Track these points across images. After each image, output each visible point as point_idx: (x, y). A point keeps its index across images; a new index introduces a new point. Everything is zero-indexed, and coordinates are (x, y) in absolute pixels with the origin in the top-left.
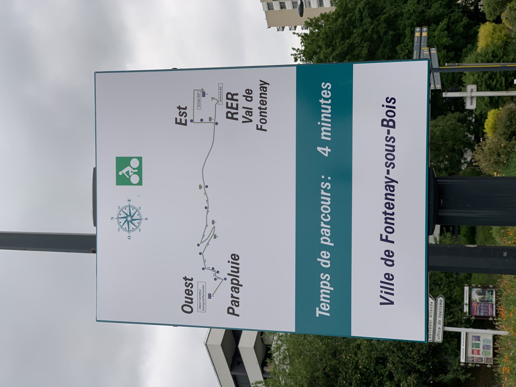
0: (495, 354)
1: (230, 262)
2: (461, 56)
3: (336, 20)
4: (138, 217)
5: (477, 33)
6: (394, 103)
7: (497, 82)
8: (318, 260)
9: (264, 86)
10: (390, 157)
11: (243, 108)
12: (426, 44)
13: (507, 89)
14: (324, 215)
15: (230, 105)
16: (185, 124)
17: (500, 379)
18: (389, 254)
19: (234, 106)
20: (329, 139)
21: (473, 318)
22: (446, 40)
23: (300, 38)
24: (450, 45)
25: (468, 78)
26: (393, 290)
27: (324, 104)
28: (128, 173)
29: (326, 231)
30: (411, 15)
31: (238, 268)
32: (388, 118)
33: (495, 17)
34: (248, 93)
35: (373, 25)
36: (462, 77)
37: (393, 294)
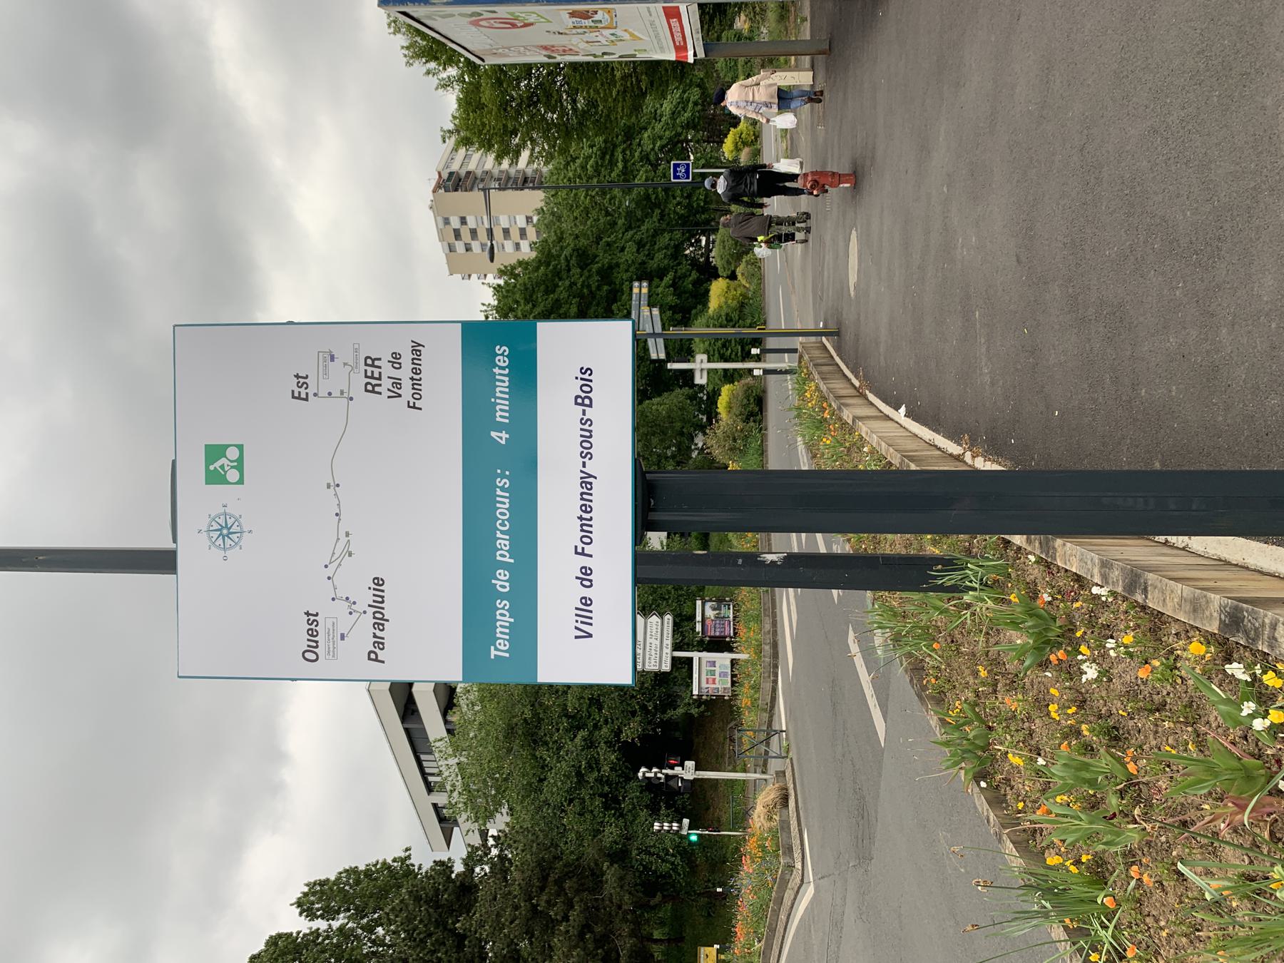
0: (733, 683)
2: (689, 319)
3: (537, 269)
4: (212, 534)
5: (708, 291)
6: (590, 375)
7: (732, 351)
8: (493, 581)
9: (417, 349)
10: (585, 445)
11: (389, 377)
12: (646, 302)
13: (743, 360)
14: (500, 521)
16: (306, 399)
17: (739, 714)
18: (586, 571)
19: (376, 375)
20: (507, 421)
21: (708, 639)
22: (671, 299)
23: (492, 289)
24: (676, 305)
25: (698, 345)
26: (591, 618)
27: (500, 374)
28: (222, 467)
29: (503, 542)
30: (629, 266)
31: (382, 597)
32: (583, 395)
33: (729, 273)
34: (396, 358)
35: (583, 278)
36: (690, 344)
37: (591, 624)
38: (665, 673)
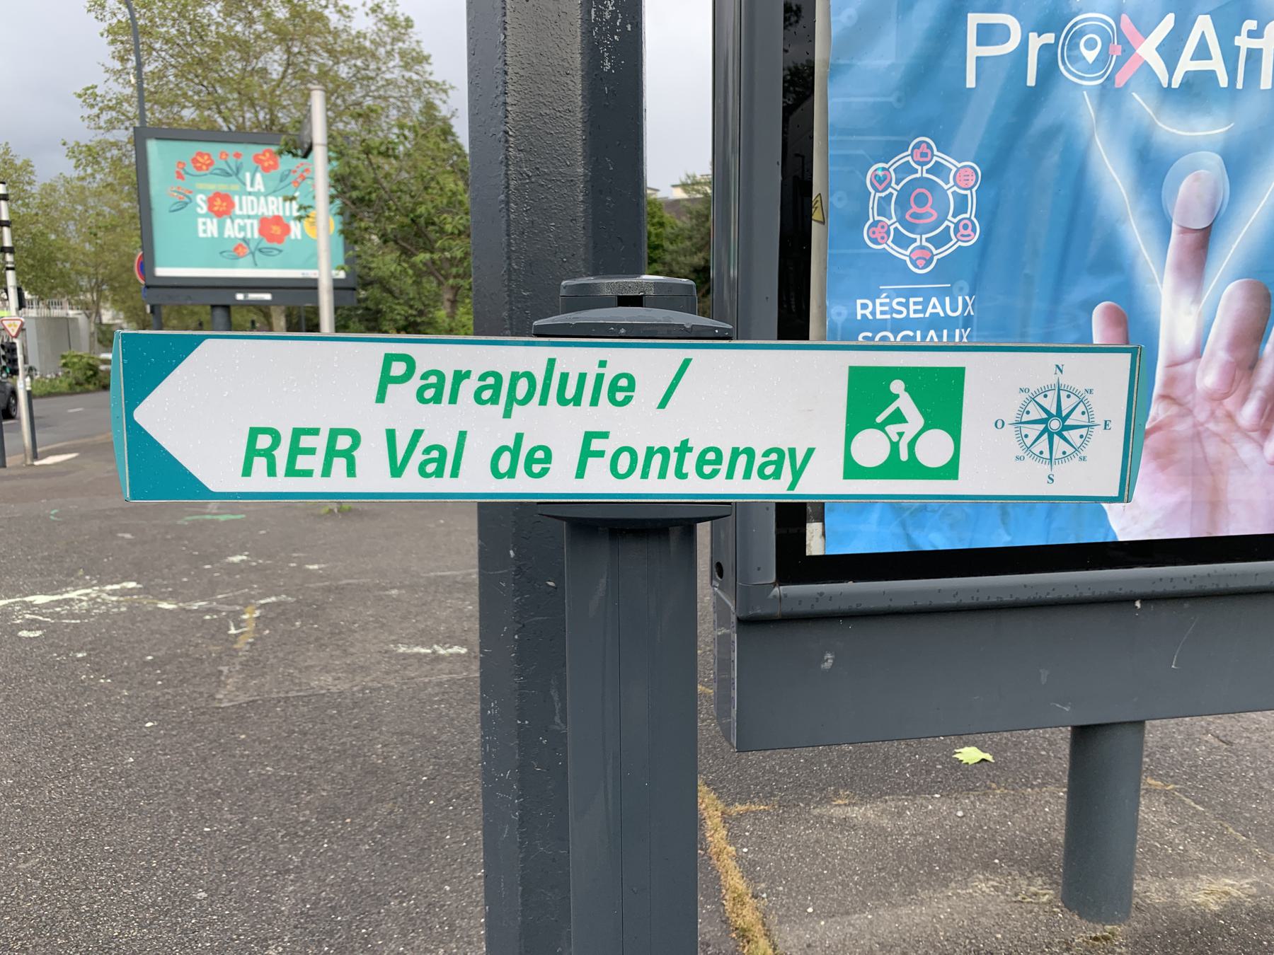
1: (601, 371)
15: (305, 441)
19: (302, 462)
31: (577, 400)
34: (530, 460)
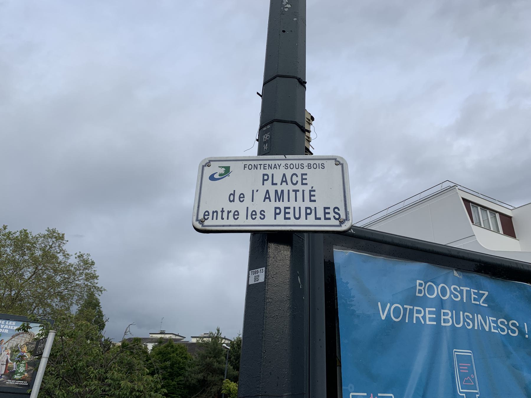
38: (7, 333)
